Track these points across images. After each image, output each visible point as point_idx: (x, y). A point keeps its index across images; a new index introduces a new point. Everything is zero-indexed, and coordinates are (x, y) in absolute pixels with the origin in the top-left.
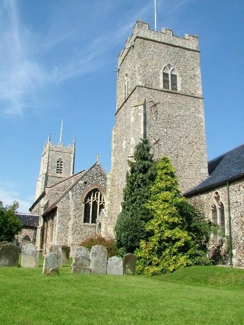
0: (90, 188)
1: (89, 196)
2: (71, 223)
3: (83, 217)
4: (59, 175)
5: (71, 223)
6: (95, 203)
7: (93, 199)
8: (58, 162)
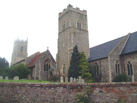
0: (46, 59)
1: (45, 62)
4: (22, 52)
5: (40, 71)
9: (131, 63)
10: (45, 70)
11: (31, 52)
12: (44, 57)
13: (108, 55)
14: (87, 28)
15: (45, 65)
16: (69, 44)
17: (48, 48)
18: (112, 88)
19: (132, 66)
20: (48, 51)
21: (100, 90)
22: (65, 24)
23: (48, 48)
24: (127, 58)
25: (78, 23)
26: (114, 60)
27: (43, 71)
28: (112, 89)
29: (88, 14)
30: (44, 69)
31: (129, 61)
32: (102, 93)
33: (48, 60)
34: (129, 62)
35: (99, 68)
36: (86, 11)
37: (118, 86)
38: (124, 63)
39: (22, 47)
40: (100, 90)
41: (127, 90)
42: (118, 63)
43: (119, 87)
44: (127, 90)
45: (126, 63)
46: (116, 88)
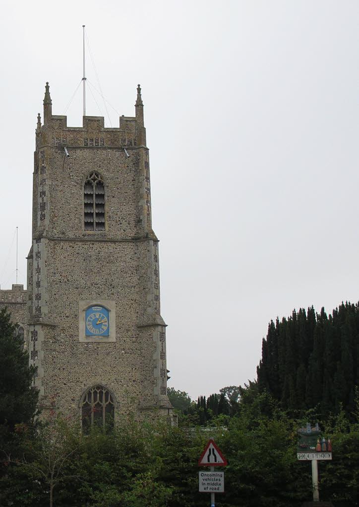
4: (95, 232)
8: (88, 184)
39: (94, 184)
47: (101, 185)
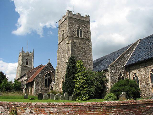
1: (46, 76)
2: (40, 87)
3: (44, 85)
6: (49, 79)
7: (48, 77)
8: (27, 60)
9: (137, 75)
10: (46, 86)
11: (36, 64)
12: (45, 71)
13: (109, 67)
14: (90, 36)
15: (46, 80)
16: (67, 56)
17: (49, 60)
18: (42, 109)
19: (139, 79)
20: (49, 64)
21: (31, 111)
22: (64, 33)
23: (49, 60)
24: (133, 70)
25: (78, 31)
26: (117, 72)
27: (44, 86)
28: (42, 110)
29: (91, 20)
30: (45, 84)
31: (135, 74)
32: (32, 114)
33: (49, 73)
34: (135, 74)
35: (50, 76)
36: (89, 17)
37: (49, 106)
38: (130, 75)
40: (31, 111)
41: (58, 112)
42: (122, 75)
43: (49, 107)
44: (58, 112)
45: (132, 75)
46: (46, 109)
47: (28, 60)
